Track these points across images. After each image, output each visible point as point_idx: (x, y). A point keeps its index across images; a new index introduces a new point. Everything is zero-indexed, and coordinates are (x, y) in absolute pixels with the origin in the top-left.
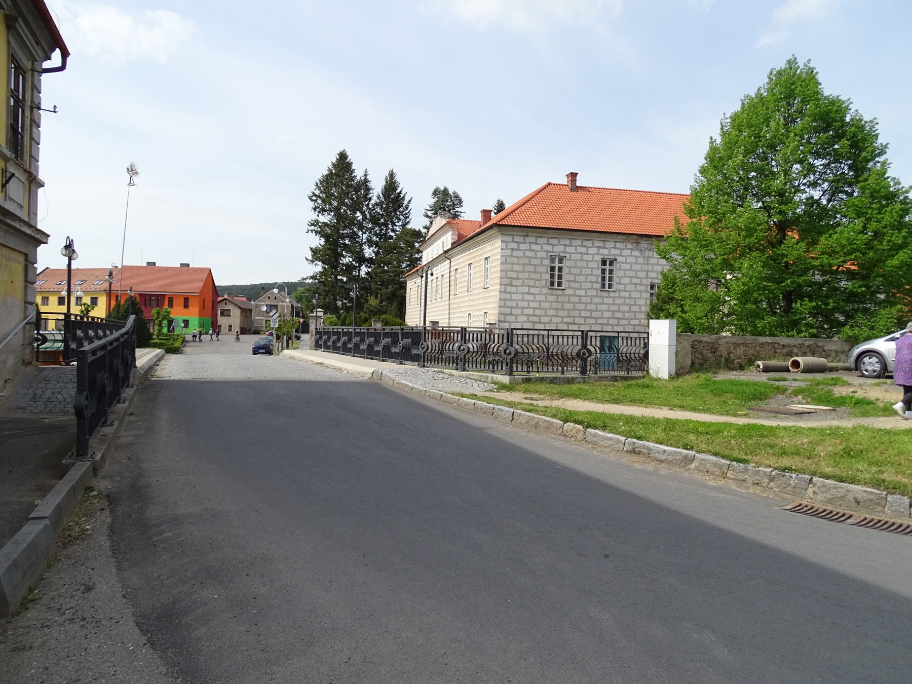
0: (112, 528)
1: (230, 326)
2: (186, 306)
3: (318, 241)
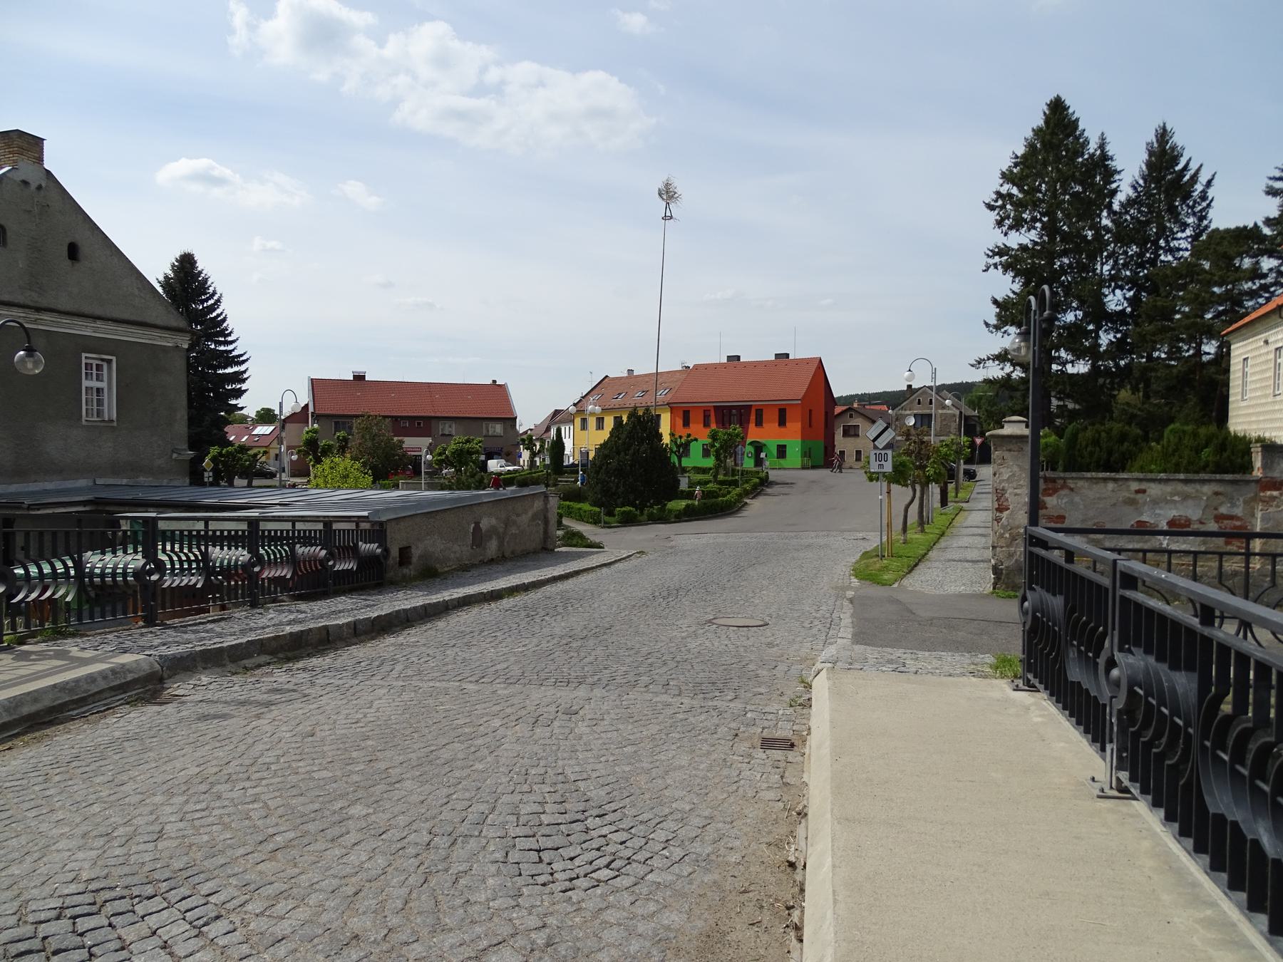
1: (858, 453)
2: (782, 422)
3: (1006, 285)
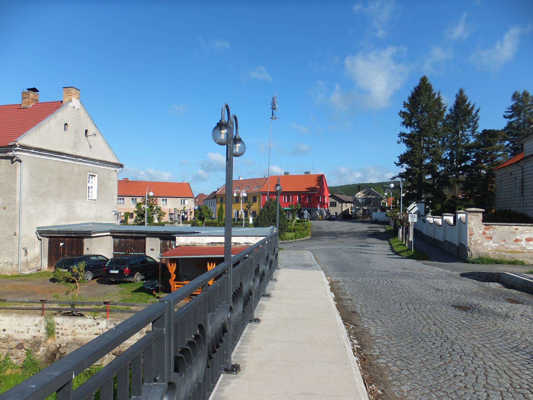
0: (71, 314)
3: (403, 149)
